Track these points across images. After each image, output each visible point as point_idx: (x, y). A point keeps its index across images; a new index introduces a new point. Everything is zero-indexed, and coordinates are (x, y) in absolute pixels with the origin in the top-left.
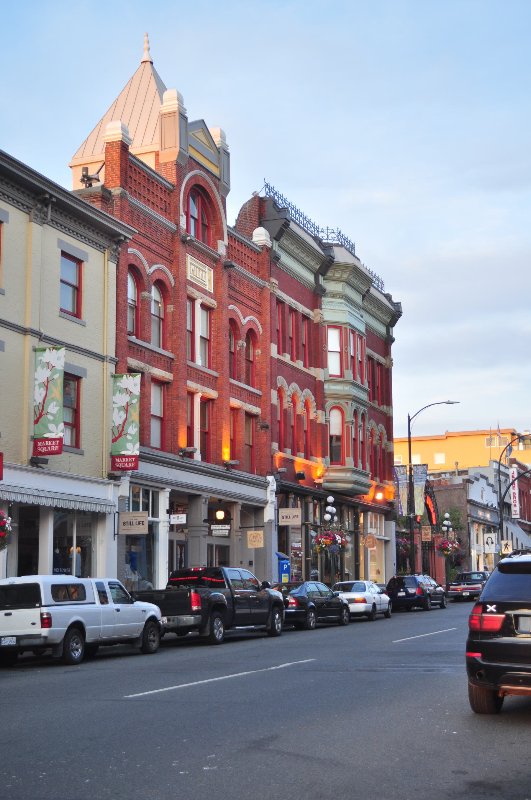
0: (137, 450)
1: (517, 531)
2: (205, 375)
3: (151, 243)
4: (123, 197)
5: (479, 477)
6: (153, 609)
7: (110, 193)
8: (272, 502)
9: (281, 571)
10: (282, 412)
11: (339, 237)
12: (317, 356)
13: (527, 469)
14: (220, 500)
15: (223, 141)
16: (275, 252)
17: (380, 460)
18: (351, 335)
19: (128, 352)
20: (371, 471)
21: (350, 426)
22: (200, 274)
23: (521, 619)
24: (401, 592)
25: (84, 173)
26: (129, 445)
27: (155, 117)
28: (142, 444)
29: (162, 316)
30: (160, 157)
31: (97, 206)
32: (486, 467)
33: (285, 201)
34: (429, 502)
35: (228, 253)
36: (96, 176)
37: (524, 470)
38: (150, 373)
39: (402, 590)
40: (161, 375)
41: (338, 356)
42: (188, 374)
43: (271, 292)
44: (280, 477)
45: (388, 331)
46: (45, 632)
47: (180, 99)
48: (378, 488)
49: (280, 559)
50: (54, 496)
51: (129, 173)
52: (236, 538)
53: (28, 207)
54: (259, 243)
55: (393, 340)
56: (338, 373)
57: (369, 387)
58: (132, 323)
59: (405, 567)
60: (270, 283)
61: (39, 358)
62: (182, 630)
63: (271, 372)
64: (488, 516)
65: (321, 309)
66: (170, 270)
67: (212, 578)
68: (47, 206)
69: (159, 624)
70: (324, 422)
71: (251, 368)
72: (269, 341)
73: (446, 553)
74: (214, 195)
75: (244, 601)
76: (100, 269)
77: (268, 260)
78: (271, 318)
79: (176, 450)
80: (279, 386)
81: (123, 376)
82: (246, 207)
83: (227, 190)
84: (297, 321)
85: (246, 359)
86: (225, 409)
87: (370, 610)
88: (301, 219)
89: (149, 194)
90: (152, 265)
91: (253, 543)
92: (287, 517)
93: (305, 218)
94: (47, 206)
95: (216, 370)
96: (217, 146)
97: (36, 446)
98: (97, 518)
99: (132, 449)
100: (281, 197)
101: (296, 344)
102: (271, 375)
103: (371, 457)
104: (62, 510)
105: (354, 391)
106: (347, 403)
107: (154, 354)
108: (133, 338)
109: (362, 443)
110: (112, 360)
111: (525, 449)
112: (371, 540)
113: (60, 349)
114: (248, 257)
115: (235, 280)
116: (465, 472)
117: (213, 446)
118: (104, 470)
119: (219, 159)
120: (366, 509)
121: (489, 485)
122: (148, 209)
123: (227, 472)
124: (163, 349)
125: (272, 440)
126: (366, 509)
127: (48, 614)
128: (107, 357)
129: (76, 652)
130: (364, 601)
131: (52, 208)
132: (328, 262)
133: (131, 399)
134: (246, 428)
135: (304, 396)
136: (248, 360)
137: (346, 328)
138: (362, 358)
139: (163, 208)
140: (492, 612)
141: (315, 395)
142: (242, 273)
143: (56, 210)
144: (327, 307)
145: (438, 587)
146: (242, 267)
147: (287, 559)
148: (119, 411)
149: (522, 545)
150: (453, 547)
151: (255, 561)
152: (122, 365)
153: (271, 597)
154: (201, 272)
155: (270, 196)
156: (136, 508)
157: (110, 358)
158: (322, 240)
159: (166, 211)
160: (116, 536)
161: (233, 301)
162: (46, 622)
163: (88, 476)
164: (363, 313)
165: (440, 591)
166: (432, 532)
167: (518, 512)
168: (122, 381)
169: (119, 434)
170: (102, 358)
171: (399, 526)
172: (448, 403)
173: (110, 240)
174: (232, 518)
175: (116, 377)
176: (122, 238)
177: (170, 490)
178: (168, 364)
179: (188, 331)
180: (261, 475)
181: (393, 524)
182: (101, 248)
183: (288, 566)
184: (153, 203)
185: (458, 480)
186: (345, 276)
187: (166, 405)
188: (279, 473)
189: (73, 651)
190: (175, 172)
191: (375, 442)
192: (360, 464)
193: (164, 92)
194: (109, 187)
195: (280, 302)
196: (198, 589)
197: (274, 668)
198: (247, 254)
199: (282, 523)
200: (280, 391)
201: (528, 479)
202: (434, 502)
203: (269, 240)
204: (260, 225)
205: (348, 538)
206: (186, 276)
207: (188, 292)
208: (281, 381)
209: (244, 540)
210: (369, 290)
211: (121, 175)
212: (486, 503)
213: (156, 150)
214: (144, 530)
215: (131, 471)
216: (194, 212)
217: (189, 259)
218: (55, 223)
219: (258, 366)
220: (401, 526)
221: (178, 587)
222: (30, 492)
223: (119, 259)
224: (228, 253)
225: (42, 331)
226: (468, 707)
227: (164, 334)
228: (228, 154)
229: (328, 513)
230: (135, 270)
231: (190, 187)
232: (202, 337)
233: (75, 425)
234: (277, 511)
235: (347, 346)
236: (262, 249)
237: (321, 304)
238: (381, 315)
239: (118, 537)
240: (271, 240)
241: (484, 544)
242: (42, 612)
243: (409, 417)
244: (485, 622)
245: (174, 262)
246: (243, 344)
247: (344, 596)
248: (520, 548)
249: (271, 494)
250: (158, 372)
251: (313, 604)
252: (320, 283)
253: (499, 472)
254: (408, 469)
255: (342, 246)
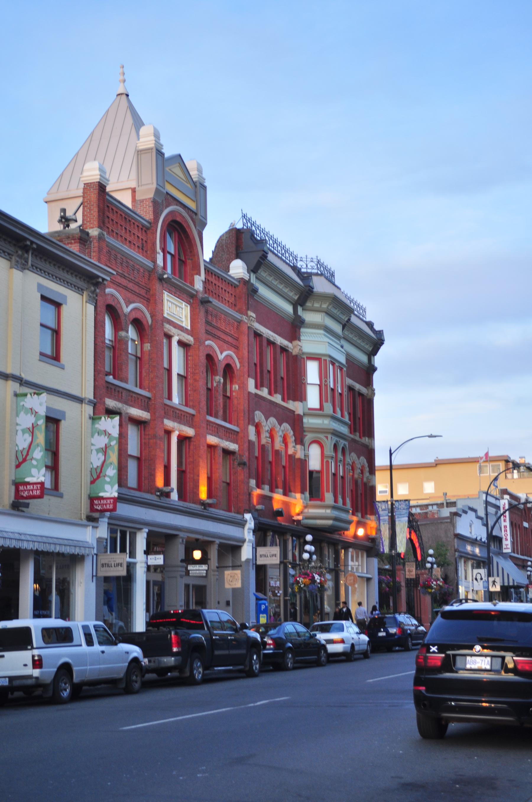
0: (116, 491)
1: (509, 567)
2: (182, 413)
3: (128, 282)
4: (100, 238)
5: (467, 509)
6: (135, 651)
7: (88, 234)
8: (250, 541)
9: (259, 611)
10: (260, 448)
11: (319, 266)
12: (296, 389)
13: (520, 499)
14: (197, 540)
15: (200, 174)
16: (252, 284)
17: (361, 494)
18: (331, 366)
19: (106, 395)
20: (352, 506)
21: (330, 461)
22: (176, 310)
23: (458, 659)
24: (381, 631)
25: (62, 214)
26: (107, 487)
27: (131, 153)
28: (120, 485)
29: (139, 355)
30: (137, 194)
31: (75, 248)
32: (475, 498)
33: (262, 231)
34: (414, 537)
35: (205, 288)
36: (74, 217)
37: (517, 501)
38: (127, 413)
39: (382, 630)
40: (138, 414)
41: (317, 389)
42: (165, 413)
43: (249, 325)
44: (257, 515)
45: (370, 360)
46: (36, 673)
47: (157, 135)
48: (360, 524)
49: (258, 599)
50: (34, 539)
51: (107, 213)
52: (212, 578)
53: (9, 254)
54: (237, 276)
55: (374, 369)
56: (317, 406)
57: (350, 420)
58: (109, 361)
59: (388, 606)
60: (247, 316)
61: (22, 404)
62: (162, 671)
63: (249, 407)
64: (477, 551)
65: (300, 340)
66: (147, 308)
67: (190, 619)
68: (27, 252)
69: (142, 665)
70: (303, 457)
71: (228, 404)
72: (246, 376)
73: (430, 590)
74: (191, 230)
75: (222, 642)
76: (78, 312)
77: (246, 293)
78: (248, 352)
79: (152, 489)
80: (257, 421)
81: (101, 418)
82: (223, 238)
83: (204, 224)
84: (275, 354)
85: (223, 395)
86: (202, 447)
87: (349, 650)
88: (279, 248)
89: (126, 232)
90: (129, 305)
91: (231, 583)
92: (265, 556)
93: (283, 247)
94: (27, 252)
95: (193, 407)
96: (194, 180)
97: (17, 491)
98: (76, 559)
99: (110, 491)
100: (258, 227)
101: (274, 378)
102: (249, 411)
103: (352, 491)
104: (43, 552)
105: (334, 424)
106: (327, 437)
107: (131, 394)
108: (110, 378)
109: (343, 478)
110: (90, 402)
111: (520, 477)
112: (352, 578)
113: (41, 394)
114: (225, 291)
115: (212, 315)
116: (453, 504)
117: (189, 485)
118: (83, 512)
119: (196, 192)
120: (347, 546)
121: (478, 517)
122: (126, 249)
123: (204, 511)
124: (140, 388)
125: (250, 477)
126: (347, 546)
127: (39, 656)
128: (85, 399)
129: (64, 692)
130: (342, 641)
131: (32, 254)
132: (307, 292)
133: (110, 441)
134: (223, 465)
135: (283, 431)
136: (225, 396)
137: (325, 360)
138: (342, 390)
139: (140, 246)
140: (434, 652)
141: (294, 429)
142: (219, 308)
143: (36, 256)
144: (306, 338)
145: (419, 626)
146: (219, 301)
147: (265, 599)
148: (97, 453)
149: (513, 581)
150: (437, 585)
151: (232, 602)
152: (101, 408)
153: (248, 638)
154: (178, 308)
155: (247, 227)
156: (114, 550)
157: (88, 400)
158: (301, 269)
159: (142, 249)
160: (94, 578)
161: (210, 337)
162: (37, 663)
163: (65, 517)
164: (343, 342)
165: (422, 631)
166: (416, 568)
167: (509, 546)
168: (100, 423)
169: (97, 476)
170: (80, 400)
171: (383, 561)
172: (431, 436)
173: (88, 282)
174: (209, 557)
175: (94, 419)
176: (100, 280)
177: (147, 530)
178: (146, 404)
179: (165, 368)
180: (238, 513)
181: (375, 561)
182: (79, 290)
183: (266, 607)
184: (130, 242)
185: (446, 512)
186: (325, 306)
187: (143, 445)
188: (257, 510)
189: (62, 691)
190: (151, 209)
191: (356, 476)
192: (340, 500)
193: (141, 127)
194: (87, 228)
195: (257, 335)
196: (178, 631)
197: (252, 705)
198: (224, 288)
199: (260, 561)
200: (258, 427)
201: (519, 510)
202: (419, 537)
203: (246, 273)
204: (237, 257)
205: (328, 576)
206: (163, 314)
207: (165, 330)
208: (259, 416)
209: (221, 580)
210: (349, 319)
211: (99, 216)
212: (474, 537)
213: (133, 187)
214: (122, 572)
215: (109, 513)
216: (171, 247)
217: (167, 296)
218: (35, 269)
219: (235, 402)
220: (386, 561)
221: (158, 629)
222: (12, 536)
223: (96, 301)
224: (205, 288)
225: (23, 376)
226: (418, 735)
227: (141, 373)
228: (205, 188)
229: (306, 552)
230: (112, 310)
231: (167, 223)
232: (178, 375)
233: (54, 467)
234: (254, 549)
235: (327, 378)
236: (239, 282)
237: (300, 335)
238: (363, 344)
239: (97, 580)
240: (248, 272)
241: (473, 580)
242: (33, 654)
243: (390, 451)
244: (429, 661)
245: (152, 301)
246: (220, 380)
247: (322, 637)
248: (511, 584)
249: (249, 532)
250: (136, 412)
251: (291, 645)
252: (299, 314)
253: (487, 503)
254: (389, 503)
255: (321, 275)
